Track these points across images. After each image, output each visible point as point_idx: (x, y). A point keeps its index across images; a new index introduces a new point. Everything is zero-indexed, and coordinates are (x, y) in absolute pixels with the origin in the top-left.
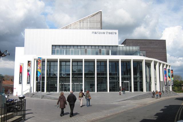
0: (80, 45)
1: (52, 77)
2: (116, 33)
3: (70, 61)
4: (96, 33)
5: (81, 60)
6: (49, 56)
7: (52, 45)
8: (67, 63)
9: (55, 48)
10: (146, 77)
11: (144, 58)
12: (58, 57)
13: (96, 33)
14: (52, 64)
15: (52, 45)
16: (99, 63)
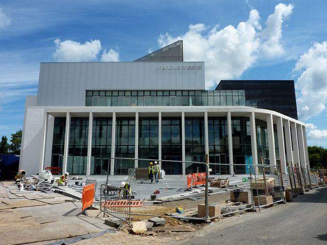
0: (143, 89)
3: (157, 118)
5: (155, 116)
6: (81, 108)
7: (87, 91)
8: (131, 122)
9: (91, 96)
10: (277, 149)
11: (254, 110)
15: (87, 91)
16: (237, 122)
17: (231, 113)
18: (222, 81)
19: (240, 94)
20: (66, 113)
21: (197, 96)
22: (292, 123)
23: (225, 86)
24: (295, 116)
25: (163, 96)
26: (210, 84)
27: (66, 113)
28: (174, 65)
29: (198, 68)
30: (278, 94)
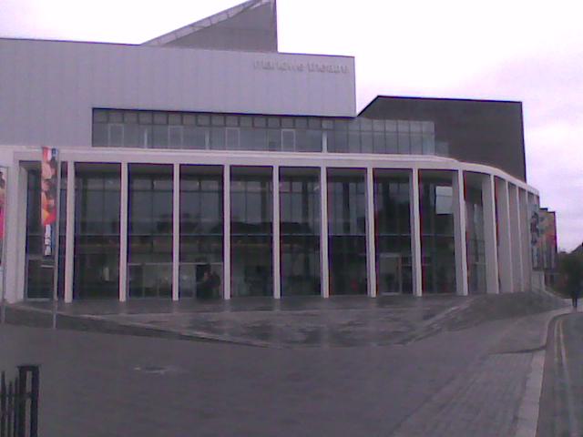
1: (95, 245)
7: (94, 110)
8: (110, 183)
9: (107, 121)
14: (94, 184)
15: (94, 110)
18: (379, 96)
19: (427, 127)
21: (334, 129)
22: (512, 185)
23: (385, 106)
24: (525, 180)
26: (362, 101)
28: (263, 57)
29: (341, 68)
30: (488, 129)
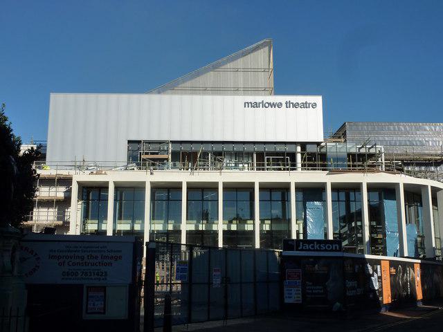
2: (314, 106)
4: (256, 105)
8: (208, 196)
12: (147, 177)
13: (256, 105)
17: (260, 183)
20: (326, 183)
25: (203, 200)
27: (326, 183)
